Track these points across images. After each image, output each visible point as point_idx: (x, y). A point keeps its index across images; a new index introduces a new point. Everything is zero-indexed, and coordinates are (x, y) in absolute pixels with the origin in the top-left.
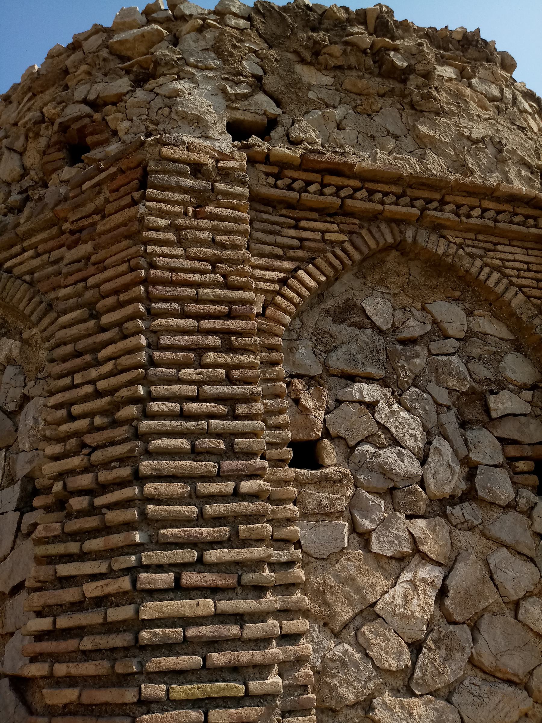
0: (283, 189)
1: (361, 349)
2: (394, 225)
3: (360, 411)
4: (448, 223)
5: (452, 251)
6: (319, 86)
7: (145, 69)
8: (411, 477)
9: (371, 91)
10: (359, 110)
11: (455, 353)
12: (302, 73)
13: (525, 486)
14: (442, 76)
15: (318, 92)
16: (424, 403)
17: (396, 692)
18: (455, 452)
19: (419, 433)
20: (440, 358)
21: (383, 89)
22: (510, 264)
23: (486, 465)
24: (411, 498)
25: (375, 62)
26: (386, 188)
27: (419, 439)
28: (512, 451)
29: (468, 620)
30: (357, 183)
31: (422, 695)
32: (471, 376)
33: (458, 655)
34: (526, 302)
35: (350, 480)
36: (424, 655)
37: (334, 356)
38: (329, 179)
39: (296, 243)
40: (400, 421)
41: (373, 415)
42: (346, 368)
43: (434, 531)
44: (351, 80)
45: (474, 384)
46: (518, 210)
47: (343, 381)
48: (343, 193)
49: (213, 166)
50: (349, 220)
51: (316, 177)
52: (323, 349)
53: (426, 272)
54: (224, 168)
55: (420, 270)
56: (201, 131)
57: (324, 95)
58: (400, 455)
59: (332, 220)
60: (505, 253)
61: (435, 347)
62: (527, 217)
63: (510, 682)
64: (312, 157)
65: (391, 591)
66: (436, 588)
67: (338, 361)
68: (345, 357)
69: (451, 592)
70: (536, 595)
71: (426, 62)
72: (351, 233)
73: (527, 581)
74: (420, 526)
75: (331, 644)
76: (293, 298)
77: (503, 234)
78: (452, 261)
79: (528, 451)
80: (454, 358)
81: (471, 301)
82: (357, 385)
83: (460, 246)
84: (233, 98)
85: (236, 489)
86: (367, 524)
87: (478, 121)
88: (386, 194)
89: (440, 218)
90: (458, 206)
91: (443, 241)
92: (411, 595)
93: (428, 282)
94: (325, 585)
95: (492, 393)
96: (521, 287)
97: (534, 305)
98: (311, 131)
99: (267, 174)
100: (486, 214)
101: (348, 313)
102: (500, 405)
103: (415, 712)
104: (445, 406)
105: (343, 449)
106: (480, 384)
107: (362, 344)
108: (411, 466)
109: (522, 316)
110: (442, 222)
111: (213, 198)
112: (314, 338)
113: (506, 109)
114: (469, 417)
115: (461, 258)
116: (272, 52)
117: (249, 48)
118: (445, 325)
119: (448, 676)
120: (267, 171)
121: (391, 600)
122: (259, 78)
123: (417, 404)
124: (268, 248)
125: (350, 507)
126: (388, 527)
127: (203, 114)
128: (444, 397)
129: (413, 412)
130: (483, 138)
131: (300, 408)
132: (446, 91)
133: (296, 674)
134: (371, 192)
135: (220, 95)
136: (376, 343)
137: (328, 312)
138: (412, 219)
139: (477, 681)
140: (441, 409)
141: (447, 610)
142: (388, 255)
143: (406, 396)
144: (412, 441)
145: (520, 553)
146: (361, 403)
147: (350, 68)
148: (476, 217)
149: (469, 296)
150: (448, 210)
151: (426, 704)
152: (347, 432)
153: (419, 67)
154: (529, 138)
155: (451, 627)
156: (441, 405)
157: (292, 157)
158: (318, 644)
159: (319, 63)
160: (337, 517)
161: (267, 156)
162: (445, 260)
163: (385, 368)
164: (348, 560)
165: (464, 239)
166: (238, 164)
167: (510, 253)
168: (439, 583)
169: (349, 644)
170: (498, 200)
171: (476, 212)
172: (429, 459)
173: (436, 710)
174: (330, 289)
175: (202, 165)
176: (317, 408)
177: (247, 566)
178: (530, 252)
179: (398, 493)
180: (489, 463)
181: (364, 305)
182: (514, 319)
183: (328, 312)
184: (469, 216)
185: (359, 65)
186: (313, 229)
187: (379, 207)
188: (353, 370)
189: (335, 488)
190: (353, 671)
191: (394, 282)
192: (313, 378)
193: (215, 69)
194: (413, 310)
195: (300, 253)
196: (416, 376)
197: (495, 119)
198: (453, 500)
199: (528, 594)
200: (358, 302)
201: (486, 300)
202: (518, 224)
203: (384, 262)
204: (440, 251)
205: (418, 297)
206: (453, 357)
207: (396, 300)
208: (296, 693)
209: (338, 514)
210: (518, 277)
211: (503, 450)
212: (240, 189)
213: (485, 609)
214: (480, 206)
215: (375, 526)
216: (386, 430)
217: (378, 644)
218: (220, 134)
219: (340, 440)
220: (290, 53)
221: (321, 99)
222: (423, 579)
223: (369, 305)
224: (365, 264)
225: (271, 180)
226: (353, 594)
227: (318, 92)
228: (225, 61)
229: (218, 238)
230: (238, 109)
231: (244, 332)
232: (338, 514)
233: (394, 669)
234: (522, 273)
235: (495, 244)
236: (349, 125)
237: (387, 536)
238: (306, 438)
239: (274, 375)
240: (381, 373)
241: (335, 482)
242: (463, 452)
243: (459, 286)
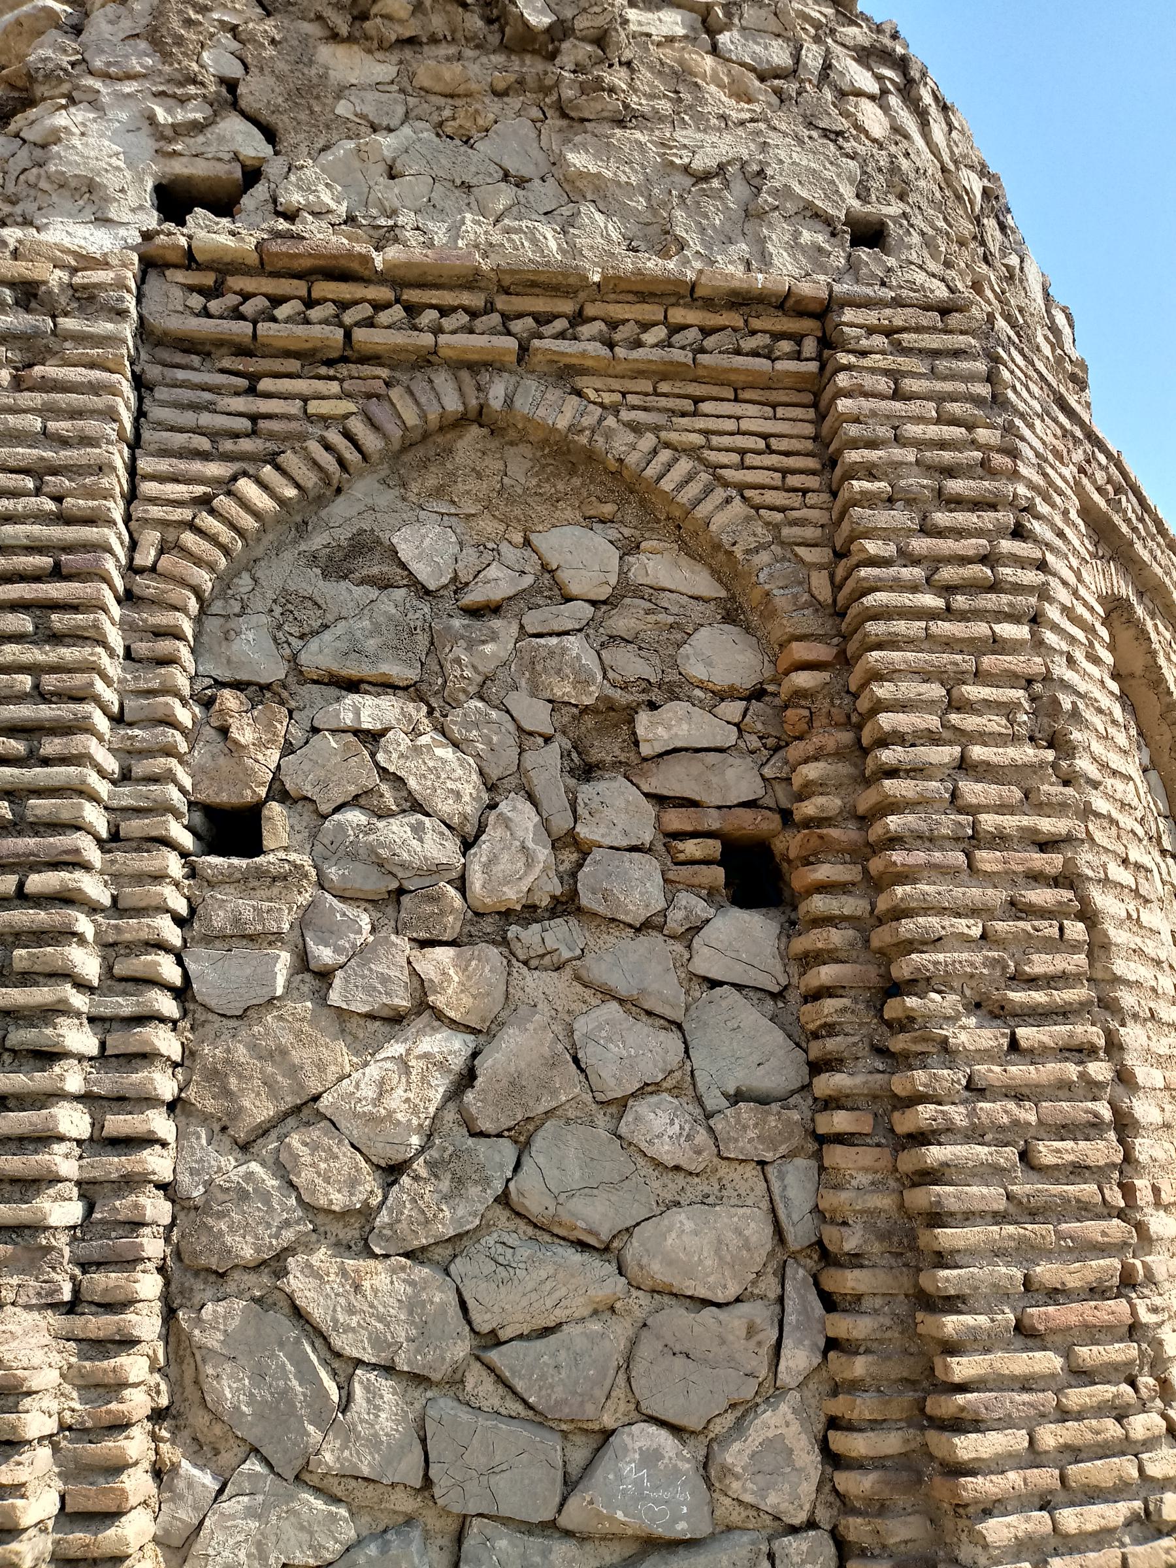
0: (221, 317)
1: (376, 630)
2: (465, 375)
4: (589, 363)
6: (362, 88)
7: (21, 90)
8: (439, 869)
9: (474, 86)
10: (449, 131)
11: (580, 630)
12: (331, 63)
13: (691, 888)
14: (649, 35)
15: (357, 101)
17: (343, 1248)
18: (545, 824)
20: (542, 641)
21: (502, 80)
23: (611, 848)
24: (428, 908)
25: (489, 21)
26: (447, 298)
27: (467, 798)
28: (676, 820)
29: (509, 1130)
30: (384, 293)
31: (387, 1256)
32: (605, 677)
33: (474, 1191)
34: (748, 519)
35: (306, 876)
36: (402, 1188)
37: (314, 644)
38: (323, 289)
39: (245, 424)
40: (431, 764)
41: (373, 755)
42: (335, 667)
43: (466, 970)
44: (432, 67)
45: (610, 692)
46: (756, 324)
47: (333, 691)
48: (349, 317)
49: (61, 285)
50: (367, 370)
51: (298, 287)
52: (295, 630)
53: (544, 467)
54: (85, 287)
56: (94, 209)
57: (369, 104)
58: (418, 830)
59: (332, 372)
61: (532, 621)
62: (777, 336)
63: (582, 1246)
64: (277, 247)
65: (356, 1075)
66: (450, 1071)
67: (320, 655)
69: (480, 1079)
70: (669, 1090)
71: (597, 9)
73: (651, 1065)
74: (438, 962)
75: (228, 1162)
76: (218, 534)
77: (718, 378)
78: (590, 442)
79: (713, 821)
80: (574, 644)
82: (351, 699)
84: (169, 132)
85: (21, 885)
86: (324, 955)
87: (719, 130)
88: (444, 311)
90: (614, 325)
93: (547, 488)
94: (227, 1061)
98: (321, 187)
99: (191, 289)
100: (677, 338)
102: (660, 731)
103: (366, 1284)
104: (540, 735)
105: (308, 818)
107: (381, 619)
108: (438, 848)
110: (574, 361)
111: (56, 348)
112: (278, 610)
113: (799, 94)
114: (596, 755)
115: (609, 435)
116: (269, 25)
117: (220, 21)
118: (563, 576)
119: (444, 1225)
120: (190, 282)
121: (352, 1089)
122: (231, 85)
123: (475, 732)
124: (179, 439)
125: (301, 925)
126: (369, 961)
127: (99, 174)
128: (537, 716)
129: (463, 747)
130: (721, 167)
131: (229, 744)
132: (651, 68)
133: (117, 1203)
134: (412, 310)
135: (146, 129)
136: (410, 616)
138: (507, 358)
139: (511, 1240)
140: (528, 742)
142: (460, 437)
143: (456, 716)
145: (649, 1013)
146: (356, 732)
147: (434, 40)
148: (653, 346)
149: (631, 512)
150: (587, 335)
151: (393, 1271)
152: (317, 789)
153: (581, 23)
154: (847, 156)
155: (470, 1142)
157: (236, 250)
158: (201, 1160)
159: (368, 38)
160: (270, 944)
161: (189, 253)
163: (422, 664)
164: (281, 1018)
165: (624, 395)
166: (112, 275)
167: (729, 417)
168: (457, 1063)
169: (263, 1164)
170: (709, 304)
173: (412, 1283)
174: (323, 513)
175: (36, 284)
176: (261, 745)
177: (24, 1018)
179: (406, 900)
181: (394, 541)
185: (453, 32)
186: (287, 394)
187: (427, 339)
188: (353, 669)
189: (275, 891)
191: (468, 492)
193: (144, 76)
195: (246, 445)
196: (487, 678)
197: (766, 121)
198: (529, 913)
199: (646, 1089)
200: (384, 537)
202: (755, 354)
208: (113, 1234)
209: (272, 938)
211: (658, 817)
212: (110, 326)
213: (549, 1114)
216: (398, 781)
218: (133, 210)
220: (311, 21)
221: (362, 116)
222: (426, 1056)
223: (406, 540)
224: (407, 458)
225: (196, 301)
226: (280, 1078)
227: (357, 101)
228: (167, 57)
229: (52, 425)
230: (181, 155)
231: (81, 604)
232: (272, 938)
234: (750, 459)
235: (697, 400)
236: (411, 166)
237: (363, 977)
238: (235, 800)
239: (155, 684)
240: (410, 674)
241: (274, 879)
242: (562, 822)
243: (613, 492)
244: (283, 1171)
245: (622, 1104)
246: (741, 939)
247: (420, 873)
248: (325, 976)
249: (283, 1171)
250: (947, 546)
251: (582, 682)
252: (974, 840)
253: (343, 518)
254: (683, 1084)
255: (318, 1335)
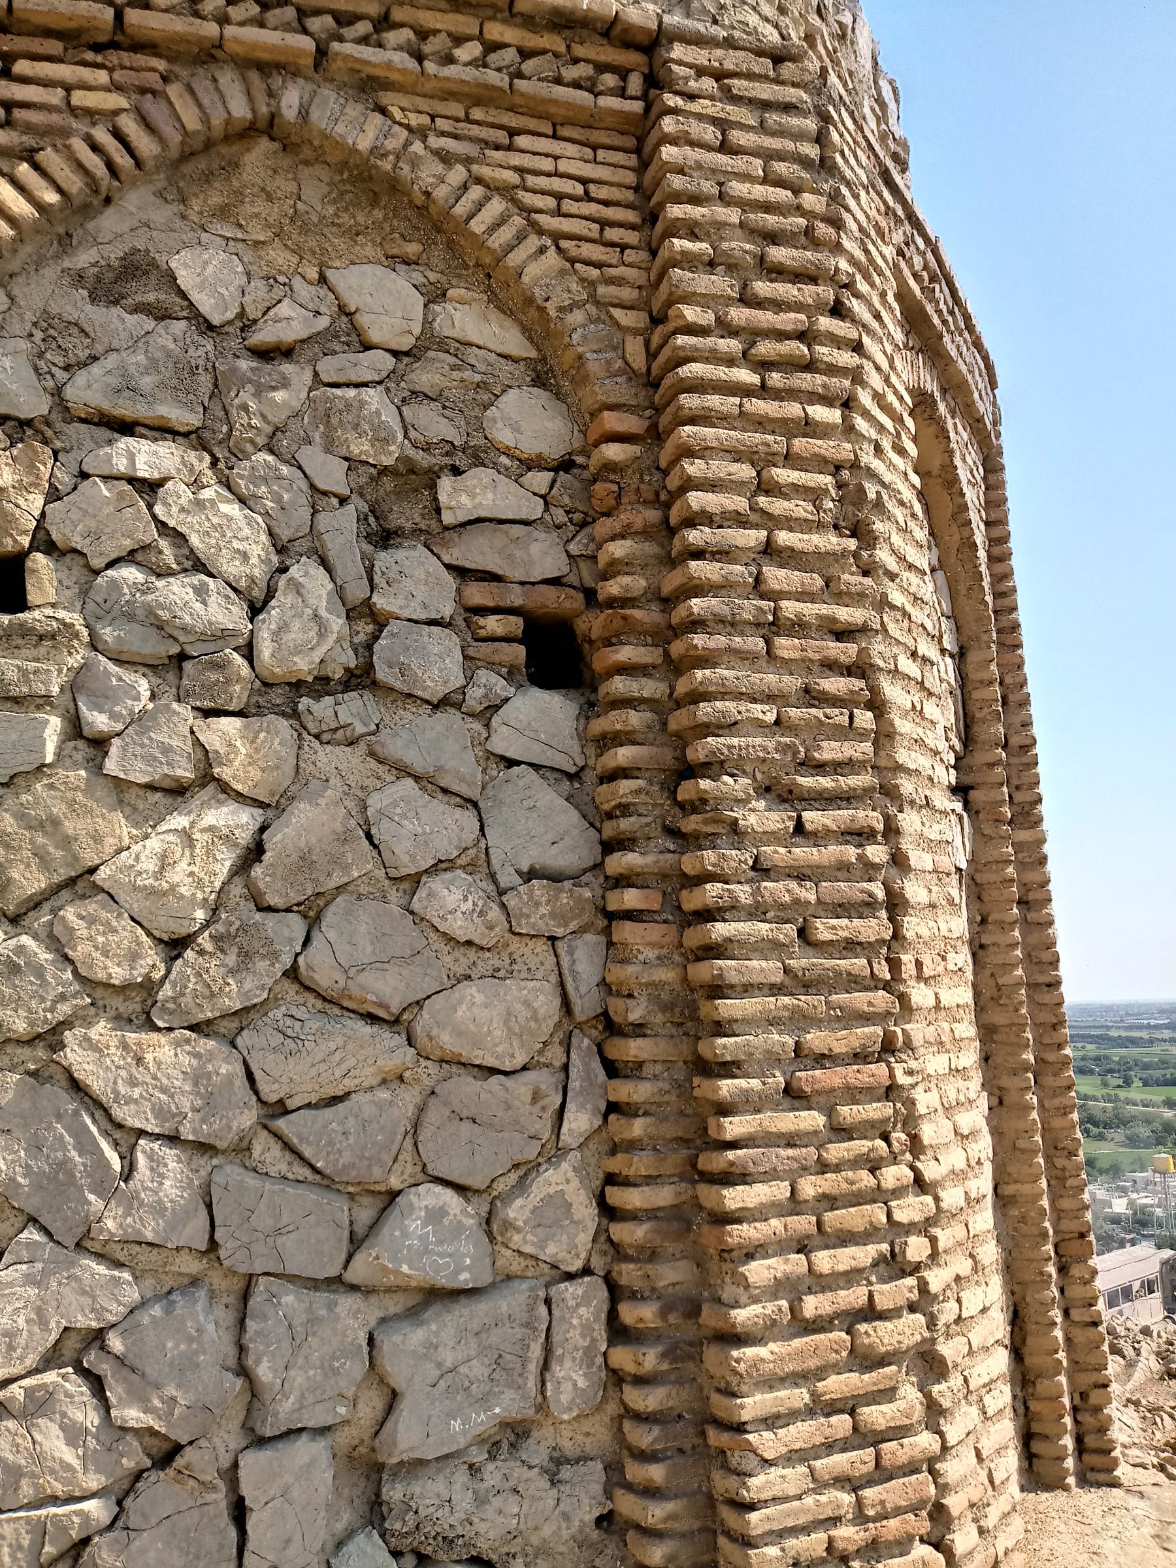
1: (152, 366)
2: (254, 76)
3: (121, 495)
4: (395, 77)
5: (391, 144)
8: (222, 635)
11: (380, 383)
13: (491, 665)
16: (280, 487)
17: (123, 1021)
18: (340, 591)
19: (258, 548)
20: (338, 392)
22: (542, 182)
23: (409, 620)
24: (213, 676)
27: (254, 560)
28: (477, 594)
29: (298, 905)
31: (170, 1029)
33: (262, 965)
34: (562, 273)
35: (77, 635)
37: (81, 377)
40: (215, 520)
41: (150, 507)
42: (106, 406)
46: (579, 51)
47: (104, 433)
50: (141, 60)
52: (59, 360)
53: (342, 194)
55: (326, 189)
58: (201, 592)
60: (535, 154)
61: (329, 368)
62: (601, 68)
63: (372, 1018)
65: (135, 848)
66: (236, 845)
67: (88, 389)
68: (109, 379)
70: (463, 867)
72: (143, 91)
73: (446, 842)
77: (535, 109)
79: (515, 597)
81: (442, 266)
83: (421, 133)
86: (99, 721)
89: (367, 63)
90: (423, 34)
91: (378, 118)
92: (178, 855)
95: (456, 471)
96: (557, 237)
97: (582, 280)
100: (493, 58)
101: (131, 280)
102: (464, 499)
103: (149, 1057)
104: (335, 496)
106: (430, 454)
107: (159, 354)
108: (224, 613)
109: (547, 304)
112: (39, 335)
114: (396, 520)
115: (415, 163)
118: (363, 320)
119: (230, 998)
121: (131, 862)
123: (264, 489)
125: (73, 688)
126: (149, 729)
129: (251, 503)
136: (191, 352)
137: (79, 278)
140: (322, 502)
141: (255, 885)
142: (248, 150)
144: (237, 563)
145: (445, 791)
146: (132, 480)
148: (466, 64)
149: (438, 254)
151: (177, 1044)
155: (258, 916)
156: (325, 493)
162: (377, 167)
163: (205, 409)
164: (51, 786)
167: (547, 155)
168: (244, 837)
169: (35, 937)
171: (468, 51)
172: (273, 603)
173: (197, 1056)
174: (91, 226)
178: (601, 154)
179: (188, 666)
180: (414, 617)
181: (173, 265)
182: (533, 313)
183: (79, 278)
184: (450, 60)
187: (211, 29)
188: (126, 409)
189: (42, 651)
190: (32, 983)
191: (257, 215)
192: (29, 423)
194: (297, 283)
196: (277, 429)
198: (321, 685)
199: (440, 866)
200: (161, 259)
201: (477, 265)
202: (576, 85)
203: (237, 165)
204: (364, 144)
205: (314, 253)
206: (371, 391)
207: (260, 257)
209: (40, 701)
210: (558, 212)
213: (340, 889)
214: (480, 37)
215: (119, 727)
216: (178, 537)
217: (90, 939)
219: (75, 556)
222: (211, 829)
223: (185, 265)
226: (51, 850)
233: (117, 982)
234: (568, 206)
235: (513, 133)
237: (142, 746)
240: (191, 419)
241: (41, 638)
242: (357, 591)
243: (418, 229)
244: (58, 945)
245: (415, 880)
246: (540, 719)
247: (203, 638)
248: (100, 743)
249: (58, 945)
250: (766, 318)
251: (382, 439)
252: (774, 627)
253: (113, 234)
254: (477, 862)
255: (98, 1106)
